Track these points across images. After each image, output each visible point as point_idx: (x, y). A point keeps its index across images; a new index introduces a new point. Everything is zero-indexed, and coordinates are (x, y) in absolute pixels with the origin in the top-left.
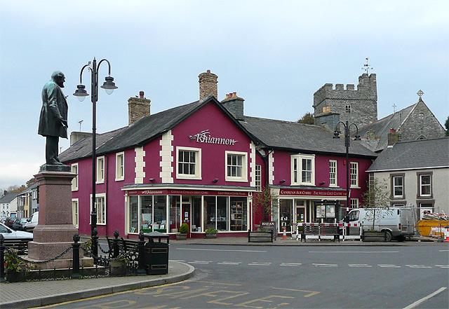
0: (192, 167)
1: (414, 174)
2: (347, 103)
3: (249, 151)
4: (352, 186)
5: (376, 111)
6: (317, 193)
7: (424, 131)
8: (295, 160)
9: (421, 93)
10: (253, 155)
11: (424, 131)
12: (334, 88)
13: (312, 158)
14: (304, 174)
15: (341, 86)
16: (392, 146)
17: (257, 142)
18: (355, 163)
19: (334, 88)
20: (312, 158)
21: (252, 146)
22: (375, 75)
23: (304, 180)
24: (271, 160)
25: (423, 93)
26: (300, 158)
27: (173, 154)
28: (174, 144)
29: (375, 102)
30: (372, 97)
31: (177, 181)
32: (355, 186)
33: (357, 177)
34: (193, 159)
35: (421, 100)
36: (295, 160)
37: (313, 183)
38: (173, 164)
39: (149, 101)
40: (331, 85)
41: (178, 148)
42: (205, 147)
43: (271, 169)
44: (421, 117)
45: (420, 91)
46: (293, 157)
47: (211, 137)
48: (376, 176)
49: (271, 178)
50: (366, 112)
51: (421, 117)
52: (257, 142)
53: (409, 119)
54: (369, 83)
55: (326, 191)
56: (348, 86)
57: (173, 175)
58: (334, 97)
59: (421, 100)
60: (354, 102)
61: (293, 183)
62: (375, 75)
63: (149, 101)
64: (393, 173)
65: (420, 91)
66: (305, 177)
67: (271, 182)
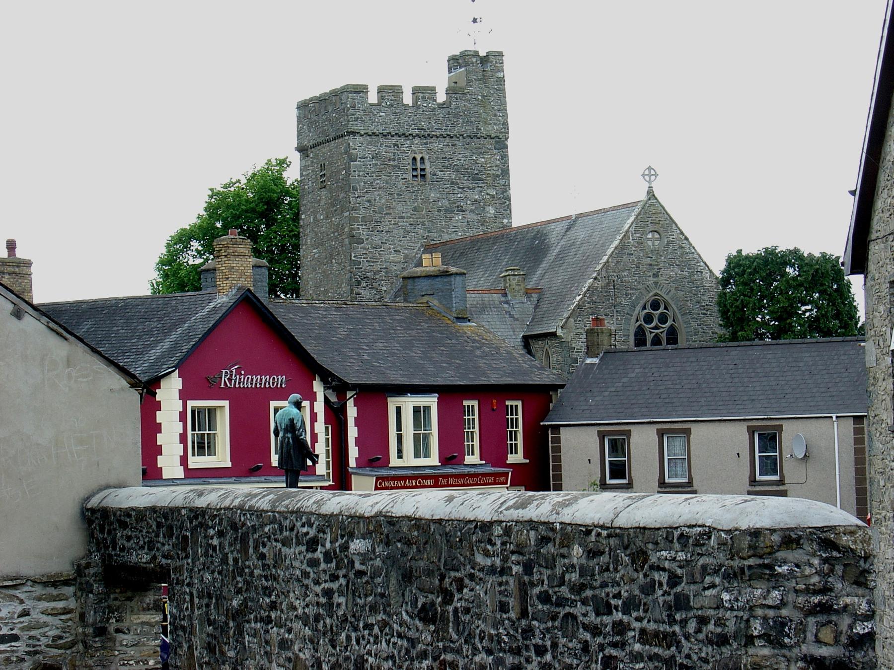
0: (211, 438)
1: (651, 434)
2: (417, 148)
3: (312, 398)
4: (512, 459)
5: (505, 173)
6: (444, 482)
7: (662, 280)
8: (399, 410)
9: (650, 173)
10: (320, 407)
11: (662, 280)
12: (373, 98)
13: (431, 401)
14: (416, 438)
15: (395, 91)
16: (596, 361)
17: (327, 377)
18: (514, 403)
19: (373, 98)
20: (431, 401)
21: (318, 387)
22: (500, 54)
23: (417, 455)
24: (352, 412)
25: (656, 175)
26: (408, 403)
27: (183, 417)
28: (185, 395)
29: (500, 143)
30: (492, 130)
31: (192, 474)
32: (517, 458)
33: (520, 436)
34: (212, 426)
35: (651, 194)
36: (399, 410)
37: (434, 460)
38: (183, 438)
39: (28, 264)
40: (361, 90)
41: (191, 404)
42: (236, 396)
43: (353, 432)
44: (651, 240)
45: (650, 168)
46: (392, 403)
47: (245, 376)
48: (564, 434)
49: (353, 452)
50: (476, 178)
51: (651, 240)
52: (327, 377)
53: (622, 247)
54: (484, 79)
55: (463, 476)
56: (416, 91)
57: (184, 460)
58: (373, 129)
59: (651, 194)
60: (436, 145)
61: (394, 461)
62: (500, 54)
63: (28, 264)
64: (602, 428)
65: (650, 168)
66: (421, 447)
67: (352, 463)
